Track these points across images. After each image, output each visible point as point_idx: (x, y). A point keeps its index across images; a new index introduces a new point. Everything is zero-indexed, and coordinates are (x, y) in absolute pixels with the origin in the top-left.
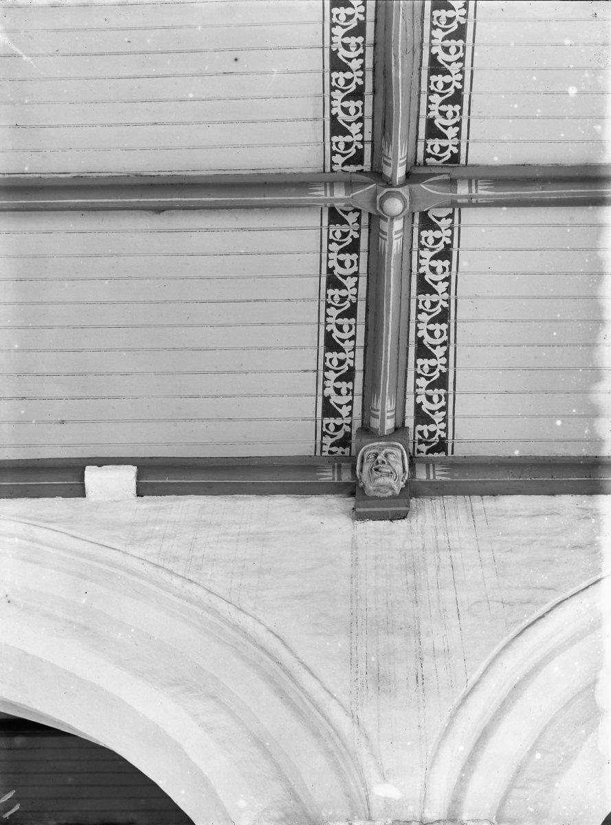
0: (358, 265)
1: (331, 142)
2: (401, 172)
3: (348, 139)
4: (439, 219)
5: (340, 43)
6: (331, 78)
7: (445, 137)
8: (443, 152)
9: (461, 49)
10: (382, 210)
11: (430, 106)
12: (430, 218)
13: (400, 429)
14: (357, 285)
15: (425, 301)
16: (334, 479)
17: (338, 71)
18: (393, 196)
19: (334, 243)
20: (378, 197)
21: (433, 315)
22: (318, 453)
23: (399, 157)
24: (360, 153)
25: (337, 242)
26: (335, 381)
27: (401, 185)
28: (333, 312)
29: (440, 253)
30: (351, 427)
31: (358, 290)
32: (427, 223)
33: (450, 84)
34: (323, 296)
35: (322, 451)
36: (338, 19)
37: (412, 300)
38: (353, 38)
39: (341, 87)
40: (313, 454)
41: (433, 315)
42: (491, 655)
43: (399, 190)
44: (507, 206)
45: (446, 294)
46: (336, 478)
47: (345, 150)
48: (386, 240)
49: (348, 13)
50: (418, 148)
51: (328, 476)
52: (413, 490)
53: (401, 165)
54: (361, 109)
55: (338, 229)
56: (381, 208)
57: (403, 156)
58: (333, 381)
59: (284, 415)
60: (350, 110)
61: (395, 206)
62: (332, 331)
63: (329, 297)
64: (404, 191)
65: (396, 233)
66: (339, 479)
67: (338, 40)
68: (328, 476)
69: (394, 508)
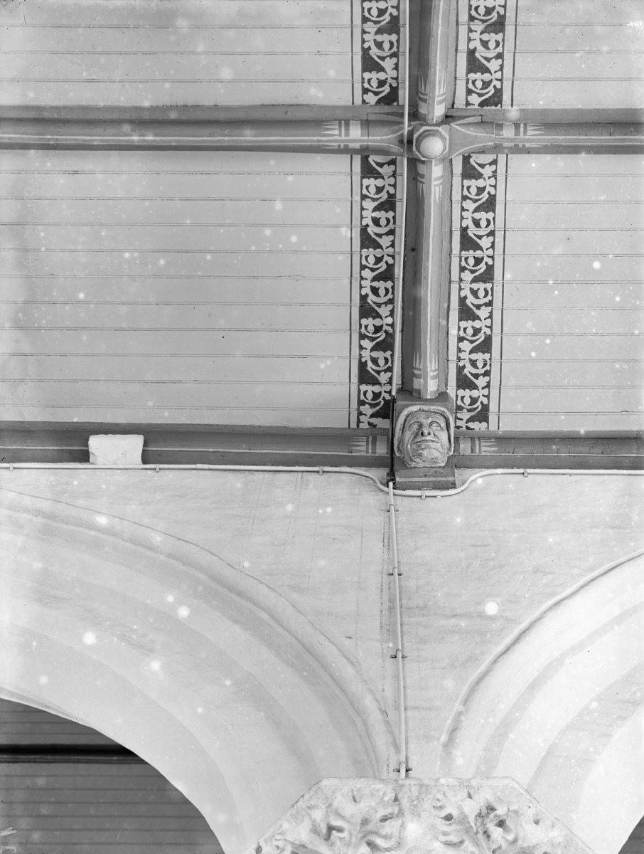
0: (393, 293)
1: (363, 79)
2: (439, 111)
3: (382, 76)
4: (482, 166)
5: (372, 42)
6: (359, 391)
7: (487, 71)
8: (475, 404)
9: (490, 292)
10: (420, 152)
11: (460, 354)
12: (472, 166)
13: (442, 396)
14: (393, 245)
15: (464, 397)
16: (367, 452)
17: (367, 383)
18: (428, 136)
19: (367, 270)
20: (415, 136)
21: (480, 202)
22: (353, 425)
23: (437, 93)
24: (395, 21)
25: (369, 404)
26: (372, 350)
27: (438, 124)
28: (367, 274)
29: (493, 24)
30: (398, 10)
31: (391, 318)
32: (470, 172)
33: (484, 188)
34: (355, 327)
35: (359, 422)
36: (368, 332)
37: (454, 233)
38: (381, 282)
39: (374, 90)
40: (351, 104)
41: (480, 202)
42: (582, 581)
43: (440, 129)
44: (544, 756)
45: (491, 250)
46: (370, 451)
47: (378, 87)
48: (424, 183)
49: (378, 185)
50: (447, 436)
51: (362, 449)
52: (457, 462)
53: (440, 102)
54: (391, 291)
55: (372, 183)
56: (418, 149)
57: (441, 93)
58: (368, 416)
59: (318, 375)
60: (376, 391)
61: (434, 147)
62: (367, 295)
63: (366, 81)
64: (442, 130)
65: (436, 179)
66: (374, 452)
67: (369, 214)
68: (362, 449)
69: (442, 480)
